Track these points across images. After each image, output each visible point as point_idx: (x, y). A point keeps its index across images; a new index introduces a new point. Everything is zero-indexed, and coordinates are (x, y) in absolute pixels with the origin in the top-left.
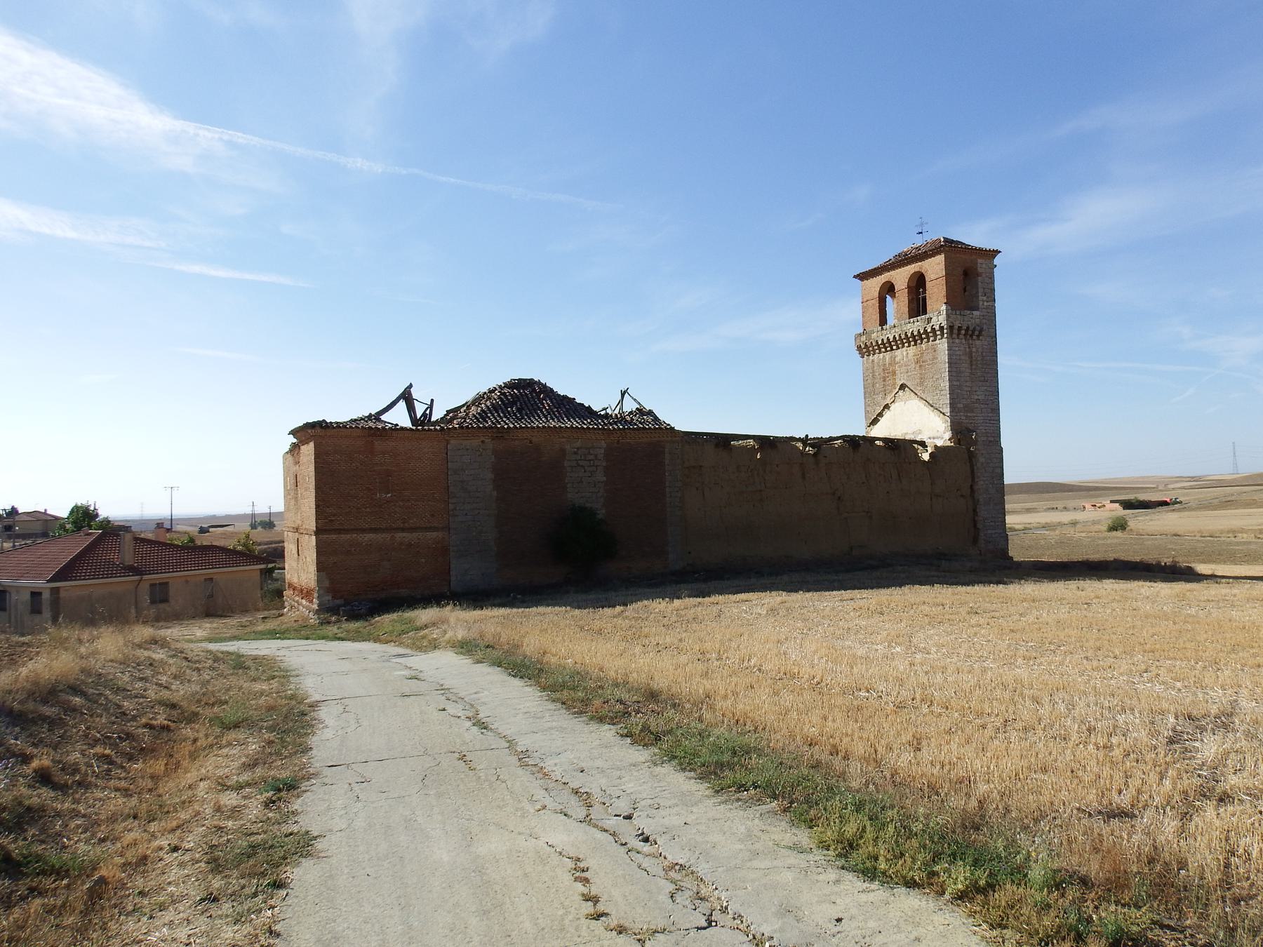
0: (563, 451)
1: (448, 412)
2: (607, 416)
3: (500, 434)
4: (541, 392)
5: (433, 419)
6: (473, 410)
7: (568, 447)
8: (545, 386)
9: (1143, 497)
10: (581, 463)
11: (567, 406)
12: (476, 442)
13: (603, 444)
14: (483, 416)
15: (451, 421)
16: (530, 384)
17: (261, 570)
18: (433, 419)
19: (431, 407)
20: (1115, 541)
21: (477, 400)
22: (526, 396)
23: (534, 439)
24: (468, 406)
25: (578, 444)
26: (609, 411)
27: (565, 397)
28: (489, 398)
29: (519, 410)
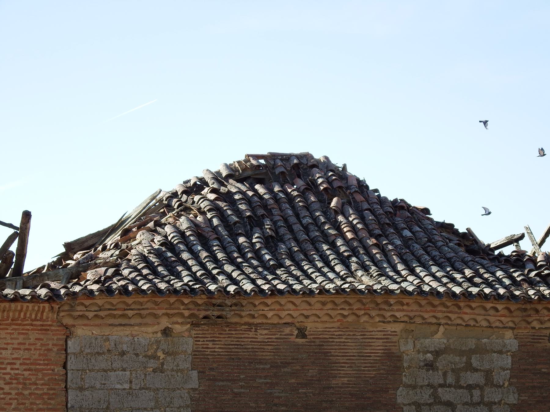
0: (393, 360)
1: (71, 248)
2: (519, 260)
3: (214, 310)
4: (330, 192)
5: (29, 266)
6: (142, 243)
7: (407, 348)
8: (342, 174)
9: (122, 328)
10: (445, 395)
11: (404, 230)
12: (147, 334)
13: (510, 340)
14: (168, 257)
15: (77, 274)
16: (298, 168)
17: (107, 246)
18: (29, 266)
19: (22, 233)
20: (269, 357)
21: (153, 215)
22: (288, 203)
23: (310, 325)
24: (125, 230)
25: (439, 339)
26: (526, 246)
27: (400, 206)
28: (185, 209)
29: (271, 242)
